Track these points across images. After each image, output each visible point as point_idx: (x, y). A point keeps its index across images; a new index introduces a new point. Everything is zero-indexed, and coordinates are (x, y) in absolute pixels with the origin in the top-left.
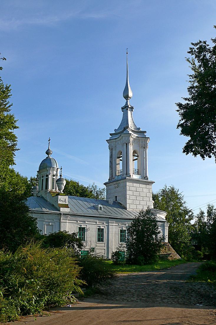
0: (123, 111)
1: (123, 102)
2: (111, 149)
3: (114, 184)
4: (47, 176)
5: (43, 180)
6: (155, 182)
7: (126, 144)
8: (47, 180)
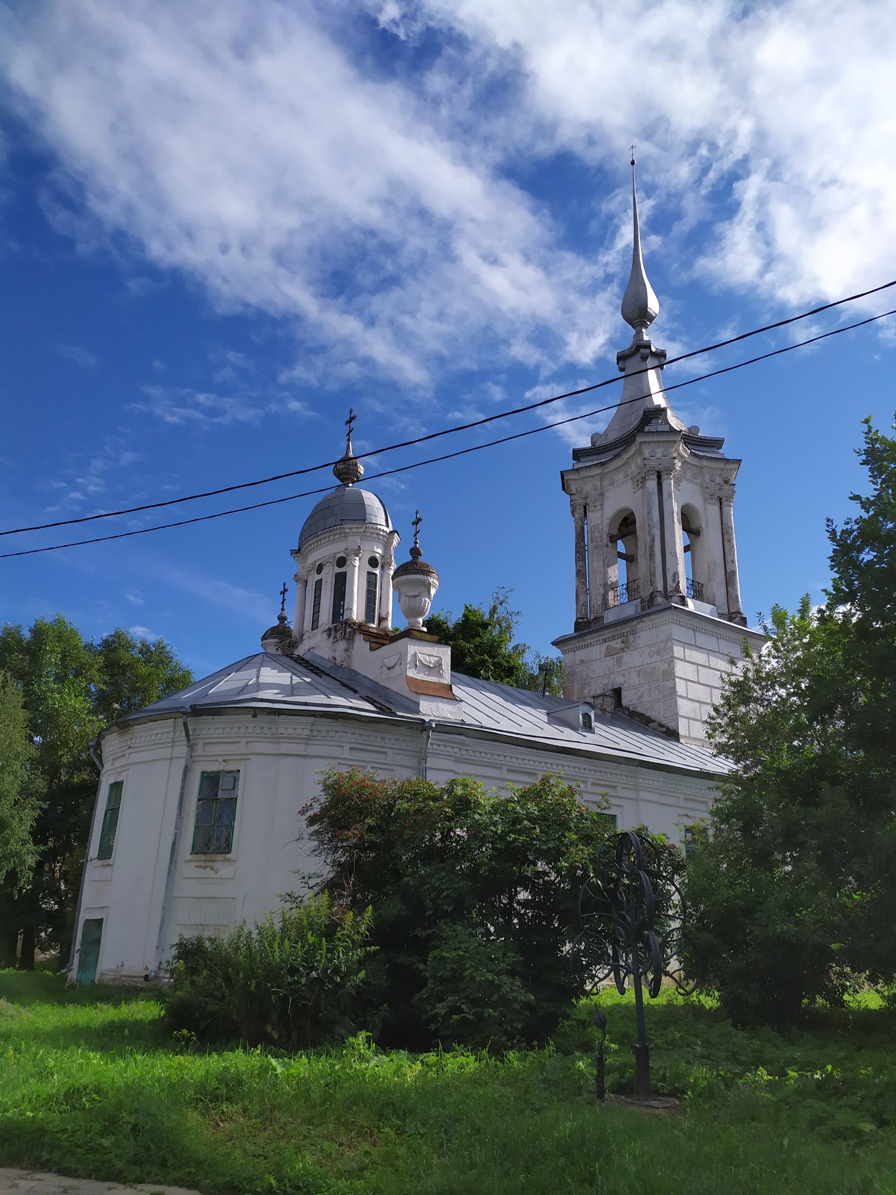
2: (582, 510)
3: (605, 641)
4: (342, 562)
5: (319, 583)
7: (720, 499)
8: (341, 582)
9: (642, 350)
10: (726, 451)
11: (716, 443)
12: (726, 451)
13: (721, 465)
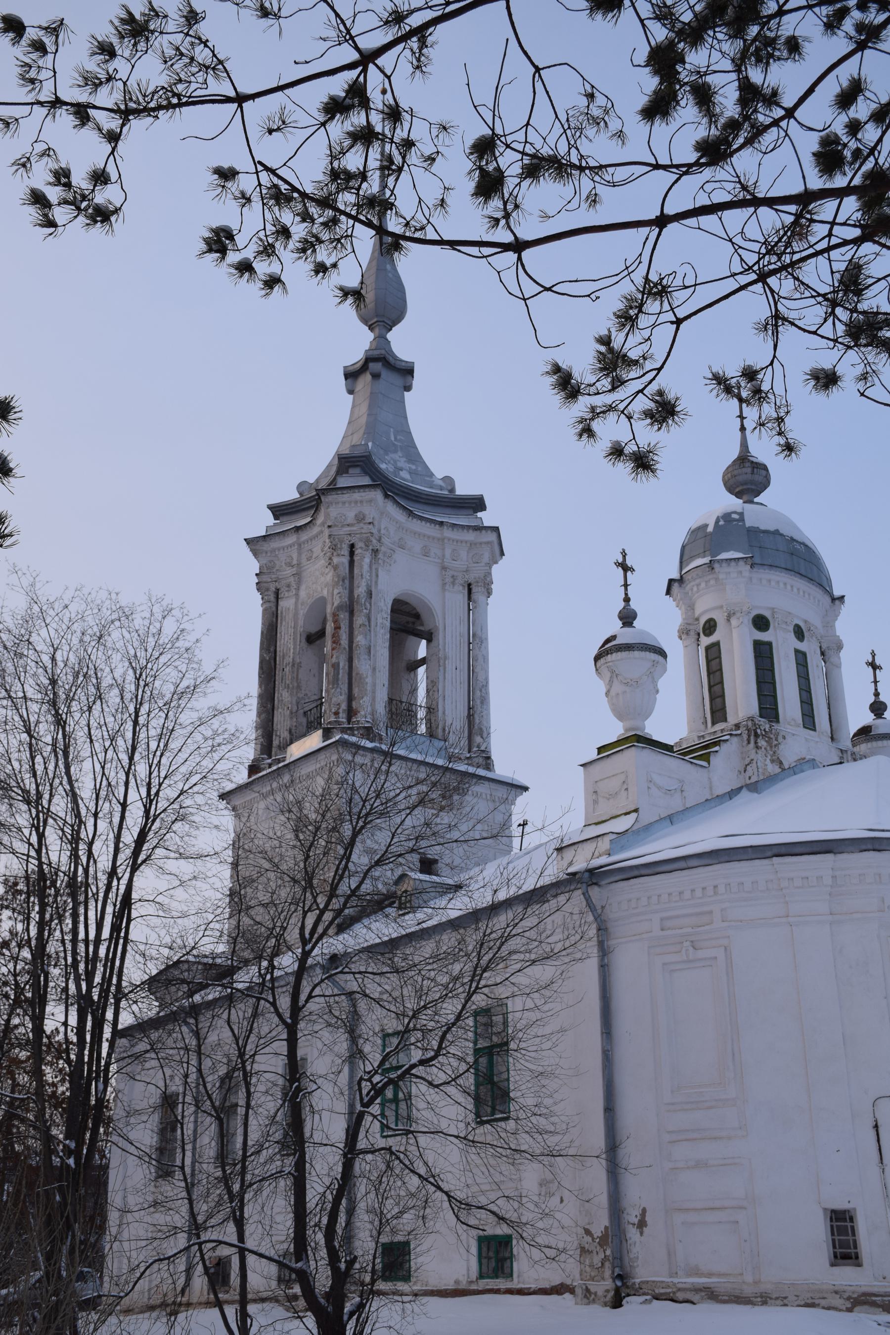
0: (351, 392)
1: (358, 341)
6: (526, 789)
9: (371, 365)
10: (487, 518)
11: (477, 504)
12: (487, 518)
13: (471, 536)
